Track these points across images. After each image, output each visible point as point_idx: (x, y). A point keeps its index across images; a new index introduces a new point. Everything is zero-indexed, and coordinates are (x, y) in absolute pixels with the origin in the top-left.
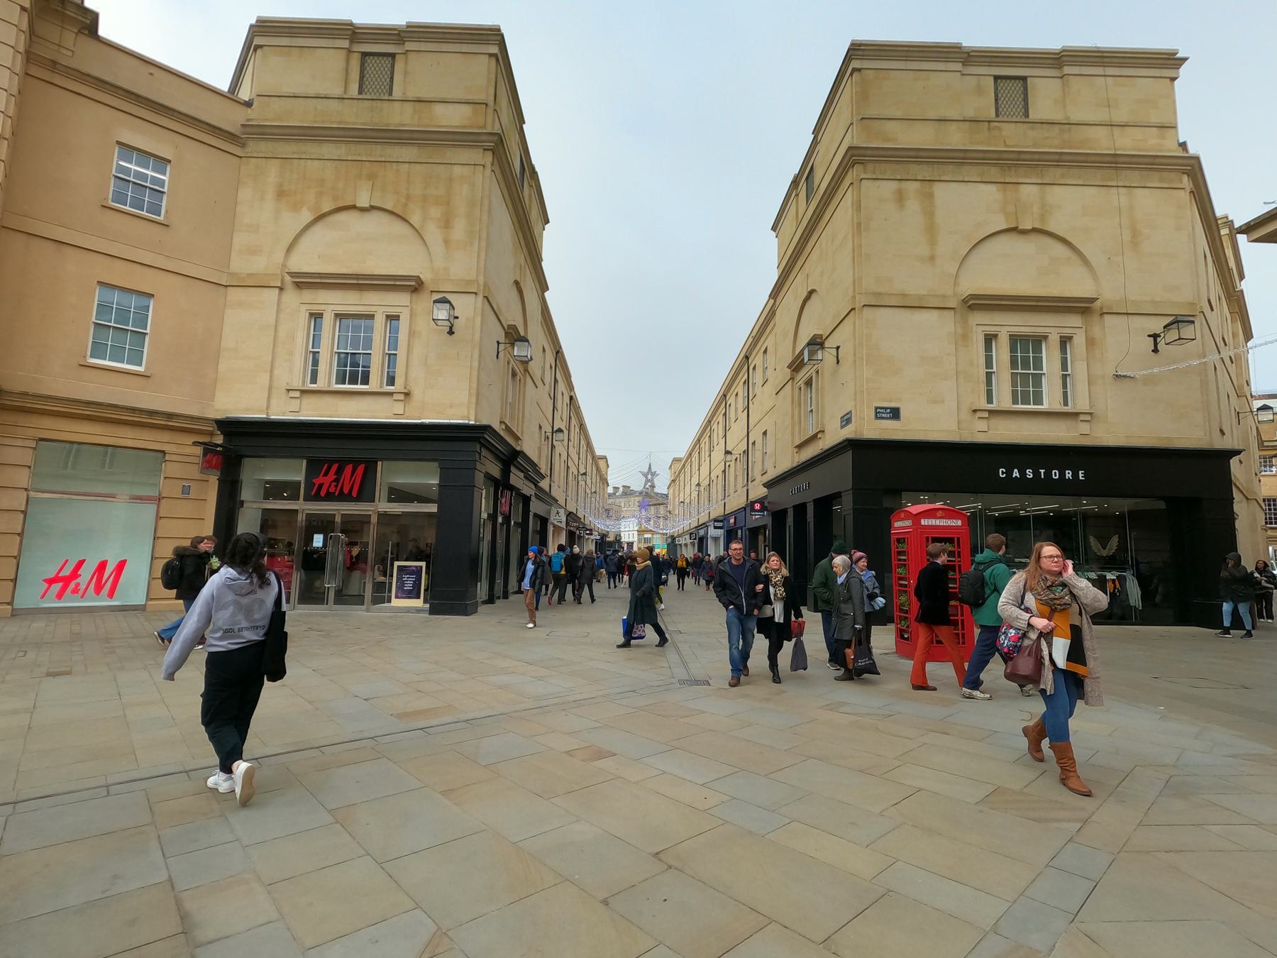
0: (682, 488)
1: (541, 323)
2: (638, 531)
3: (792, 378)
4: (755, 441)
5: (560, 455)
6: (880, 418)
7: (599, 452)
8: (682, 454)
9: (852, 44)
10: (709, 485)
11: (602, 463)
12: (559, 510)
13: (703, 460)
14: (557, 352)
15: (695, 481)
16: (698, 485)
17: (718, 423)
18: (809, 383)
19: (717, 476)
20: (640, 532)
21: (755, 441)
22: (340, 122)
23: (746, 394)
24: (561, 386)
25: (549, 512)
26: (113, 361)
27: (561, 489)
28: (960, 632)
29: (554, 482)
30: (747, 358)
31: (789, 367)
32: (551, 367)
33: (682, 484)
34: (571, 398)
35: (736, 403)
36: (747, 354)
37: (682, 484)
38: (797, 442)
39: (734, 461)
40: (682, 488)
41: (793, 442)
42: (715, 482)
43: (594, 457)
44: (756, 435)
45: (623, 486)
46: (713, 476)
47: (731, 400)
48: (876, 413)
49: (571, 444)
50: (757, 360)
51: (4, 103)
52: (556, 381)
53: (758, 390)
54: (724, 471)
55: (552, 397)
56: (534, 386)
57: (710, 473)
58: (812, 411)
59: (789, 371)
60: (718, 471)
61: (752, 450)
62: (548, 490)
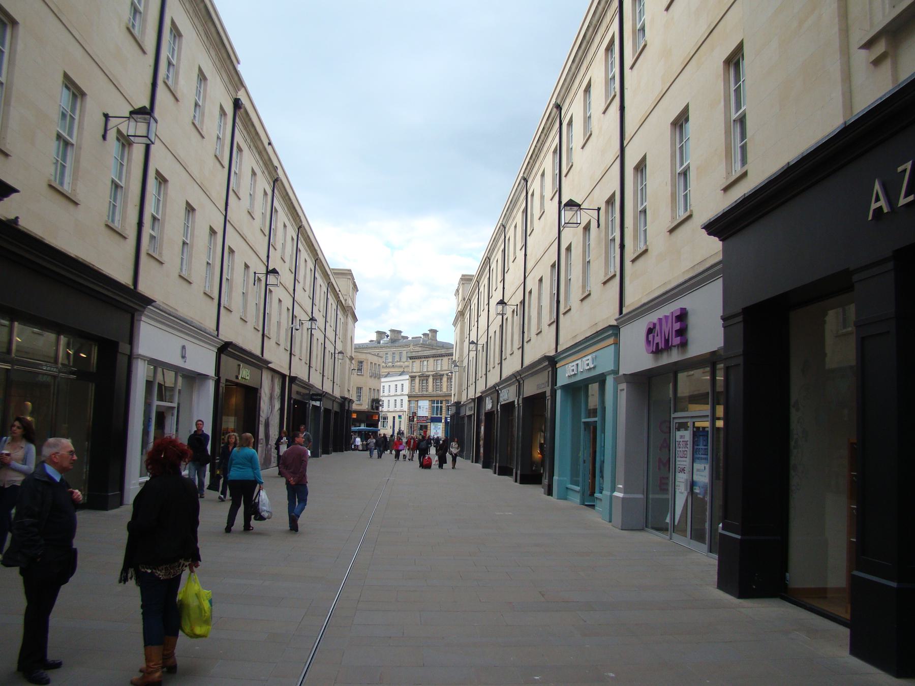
0: (474, 322)
4: (570, 245)
7: (334, 257)
10: (523, 302)
11: (341, 285)
13: (511, 259)
15: (497, 297)
16: (502, 302)
17: (516, 227)
21: (570, 245)
22: (253, 246)
23: (557, 171)
27: (318, 371)
28: (156, 403)
29: (316, 305)
30: (558, 107)
33: (474, 313)
34: (237, 104)
36: (559, 102)
37: (474, 313)
40: (474, 322)
42: (577, 252)
44: (532, 284)
46: (491, 333)
47: (535, 185)
52: (273, 210)
53: (579, 157)
54: (502, 326)
60: (495, 327)
62: (258, 353)
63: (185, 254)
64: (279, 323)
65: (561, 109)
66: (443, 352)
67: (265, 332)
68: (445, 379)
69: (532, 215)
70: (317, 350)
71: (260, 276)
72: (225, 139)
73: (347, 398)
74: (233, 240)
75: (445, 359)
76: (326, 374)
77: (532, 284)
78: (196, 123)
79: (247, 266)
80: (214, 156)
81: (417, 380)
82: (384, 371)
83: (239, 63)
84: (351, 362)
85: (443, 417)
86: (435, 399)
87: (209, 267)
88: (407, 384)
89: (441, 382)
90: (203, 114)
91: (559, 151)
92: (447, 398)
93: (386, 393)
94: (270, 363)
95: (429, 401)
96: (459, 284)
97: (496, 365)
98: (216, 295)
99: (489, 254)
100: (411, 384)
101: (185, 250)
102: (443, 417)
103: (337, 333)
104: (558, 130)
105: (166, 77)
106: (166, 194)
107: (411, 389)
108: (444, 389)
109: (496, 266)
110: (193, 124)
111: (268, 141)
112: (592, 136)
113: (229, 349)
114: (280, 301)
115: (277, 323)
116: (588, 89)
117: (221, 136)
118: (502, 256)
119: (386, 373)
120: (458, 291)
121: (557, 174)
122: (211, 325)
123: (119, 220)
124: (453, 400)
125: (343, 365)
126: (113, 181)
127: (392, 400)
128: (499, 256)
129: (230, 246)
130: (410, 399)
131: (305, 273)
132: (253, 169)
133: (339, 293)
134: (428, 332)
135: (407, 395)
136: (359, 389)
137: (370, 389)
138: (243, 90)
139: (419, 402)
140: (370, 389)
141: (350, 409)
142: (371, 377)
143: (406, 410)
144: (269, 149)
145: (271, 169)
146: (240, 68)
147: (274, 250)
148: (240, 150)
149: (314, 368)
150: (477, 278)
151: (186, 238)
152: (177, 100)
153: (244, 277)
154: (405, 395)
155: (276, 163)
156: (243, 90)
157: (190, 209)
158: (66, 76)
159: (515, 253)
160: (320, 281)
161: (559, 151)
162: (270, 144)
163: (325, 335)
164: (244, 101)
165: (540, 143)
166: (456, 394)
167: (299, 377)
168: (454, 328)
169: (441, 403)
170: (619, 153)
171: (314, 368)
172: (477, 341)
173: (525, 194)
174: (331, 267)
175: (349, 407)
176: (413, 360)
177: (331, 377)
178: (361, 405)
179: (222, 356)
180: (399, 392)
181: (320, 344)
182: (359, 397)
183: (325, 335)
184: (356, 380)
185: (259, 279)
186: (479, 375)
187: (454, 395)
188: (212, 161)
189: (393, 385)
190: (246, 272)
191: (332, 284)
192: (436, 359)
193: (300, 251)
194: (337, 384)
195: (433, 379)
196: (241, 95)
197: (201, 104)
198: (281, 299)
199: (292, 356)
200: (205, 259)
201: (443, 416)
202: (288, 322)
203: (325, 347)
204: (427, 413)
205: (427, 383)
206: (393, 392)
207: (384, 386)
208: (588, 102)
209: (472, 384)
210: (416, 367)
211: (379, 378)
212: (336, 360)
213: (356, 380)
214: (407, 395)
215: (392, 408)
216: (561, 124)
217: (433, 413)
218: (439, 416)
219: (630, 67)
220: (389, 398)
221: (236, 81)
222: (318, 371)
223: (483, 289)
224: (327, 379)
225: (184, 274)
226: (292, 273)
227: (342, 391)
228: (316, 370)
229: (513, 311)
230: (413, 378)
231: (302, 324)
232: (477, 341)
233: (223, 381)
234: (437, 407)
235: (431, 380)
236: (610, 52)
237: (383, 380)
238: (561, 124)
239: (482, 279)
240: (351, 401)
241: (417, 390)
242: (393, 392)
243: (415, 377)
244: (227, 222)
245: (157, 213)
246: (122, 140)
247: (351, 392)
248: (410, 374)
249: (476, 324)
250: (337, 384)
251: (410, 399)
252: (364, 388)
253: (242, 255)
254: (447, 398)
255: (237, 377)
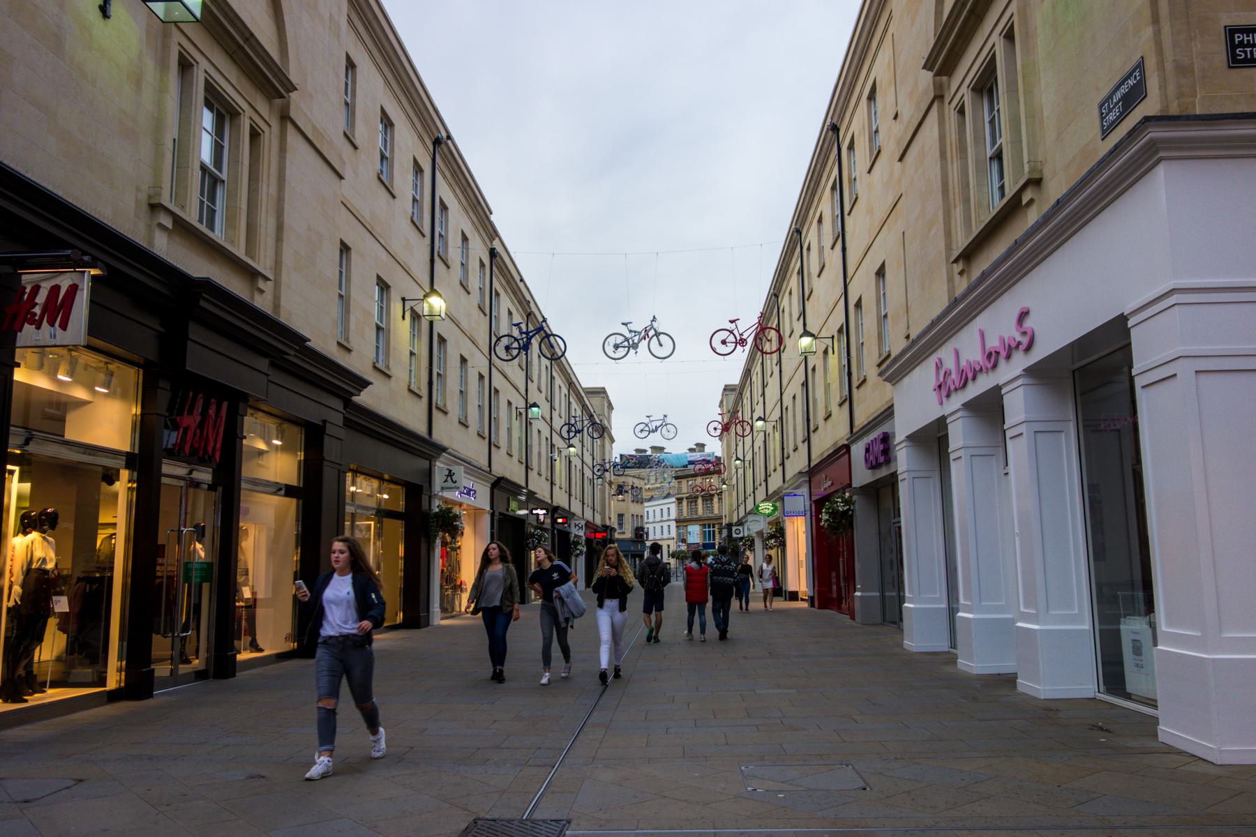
1: (350, 21)
2: (677, 521)
3: (939, 97)
4: (815, 366)
5: (576, 466)
6: (1245, 60)
8: (735, 380)
9: (726, 386)
10: (781, 418)
11: (594, 403)
12: (455, 469)
13: (769, 374)
14: (437, 142)
17: (790, 293)
18: (985, 86)
19: (794, 397)
20: (681, 522)
21: (815, 366)
24: (458, 220)
25: (429, 474)
26: (1027, 628)
29: (532, 381)
30: (835, 129)
31: (928, 66)
32: (547, 368)
34: (493, 253)
35: (818, 237)
36: (835, 121)
38: (961, 241)
39: (820, 354)
41: (949, 247)
43: (571, 384)
44: (862, 285)
45: (651, 448)
46: (756, 449)
48: (1232, 47)
49: (585, 449)
50: (857, 125)
51: (857, 566)
54: (805, 384)
55: (549, 399)
56: (334, 176)
57: (781, 394)
58: (998, 156)
59: (928, 76)
61: (856, 319)
63: (381, 341)
64: (539, 454)
65: (838, 130)
66: (713, 467)
67: (493, 440)
68: (716, 499)
69: (809, 274)
70: (576, 477)
71: (521, 411)
72: (423, 202)
73: (609, 526)
74: (498, 381)
75: (716, 476)
76: (586, 501)
77: (787, 401)
78: (384, 178)
79: (510, 403)
80: (451, 267)
81: (685, 502)
82: (646, 495)
83: (491, 213)
84: (611, 487)
85: (717, 543)
86: (707, 522)
87: (439, 378)
88: (673, 508)
89: (712, 504)
90: (392, 166)
91: (801, 272)
92: (719, 521)
93: (651, 520)
94: (536, 494)
95: (700, 525)
96: (723, 395)
97: (763, 482)
98: (424, 393)
99: (836, 117)
100: (679, 507)
101: (381, 336)
102: (717, 543)
103: (595, 457)
104: (837, 157)
105: (379, 172)
106: (445, 352)
107: (679, 513)
108: (716, 511)
109: (756, 378)
110: (380, 179)
111: (519, 278)
112: (826, 267)
113: (501, 484)
114: (539, 431)
115: (507, 430)
116: (820, 221)
117: (418, 198)
118: (798, 283)
119: (649, 497)
120: (722, 402)
121: (837, 216)
122: (483, 462)
123: (342, 332)
124: (725, 521)
125: (603, 491)
126: (377, 324)
127: (658, 526)
128: (759, 368)
129: (344, 240)
130: (678, 524)
131: (540, 370)
132: (415, 161)
133: (594, 414)
134: (695, 447)
135: (675, 520)
136: (621, 516)
137: (633, 515)
138: (497, 239)
139: (688, 527)
140: (633, 515)
141: (613, 538)
142: (633, 501)
143: (675, 537)
144: (521, 285)
145: (524, 303)
146: (493, 218)
147: (466, 294)
148: (497, 294)
149: (558, 486)
150: (832, 118)
151: (413, 348)
152: (355, 148)
153: (341, 266)
154: (672, 520)
155: (528, 298)
156: (497, 239)
157: (463, 360)
158: (379, 277)
159: (772, 368)
160: (559, 381)
161: (801, 272)
162: (522, 280)
163: (583, 461)
164: (499, 249)
165: (822, 156)
166: (727, 516)
167: (561, 506)
168: (720, 443)
169: (714, 527)
170: (780, 398)
171: (558, 486)
172: (744, 457)
173: (837, 152)
174: (584, 386)
175: (611, 536)
176: (679, 480)
177: (564, 485)
178: (624, 533)
179: (495, 490)
180: (665, 518)
181: (578, 471)
182: (621, 525)
183: (551, 427)
184: (615, 506)
185: (521, 414)
186: (748, 493)
187: (725, 516)
188: (476, 313)
189: (658, 510)
190: (463, 369)
191: (587, 405)
192: (704, 477)
193: (554, 378)
194: (561, 488)
195: (703, 501)
196: (496, 244)
197: (388, 156)
198: (466, 357)
199: (529, 471)
200: (476, 403)
201: (717, 541)
202: (547, 451)
203: (583, 474)
204: (699, 539)
205: (696, 505)
206: (658, 518)
207: (648, 512)
208: (853, 162)
209: (760, 485)
210: (685, 486)
211: (642, 503)
212: (595, 485)
213: (615, 506)
214: (675, 520)
215: (666, 535)
216: (802, 248)
217: (705, 538)
218: (712, 542)
219: (867, 170)
220: (654, 525)
221: (491, 232)
222: (563, 490)
223: (746, 402)
224: (536, 476)
225: (380, 365)
226: (523, 370)
227: (603, 519)
228: (539, 474)
229: (774, 427)
230: (680, 500)
231: (561, 451)
232: (744, 457)
233: (497, 513)
234: (709, 531)
235: (700, 501)
236: (873, 103)
237: (646, 504)
238: (802, 248)
239: (753, 369)
240: (613, 530)
241: (685, 514)
242: (658, 518)
243: (682, 499)
244: (492, 366)
245: (381, 322)
246: (380, 284)
247: (612, 520)
248: (677, 496)
249: (761, 400)
250: (588, 506)
251: (678, 524)
252: (626, 515)
253: (507, 393)
254: (719, 521)
255: (508, 510)
